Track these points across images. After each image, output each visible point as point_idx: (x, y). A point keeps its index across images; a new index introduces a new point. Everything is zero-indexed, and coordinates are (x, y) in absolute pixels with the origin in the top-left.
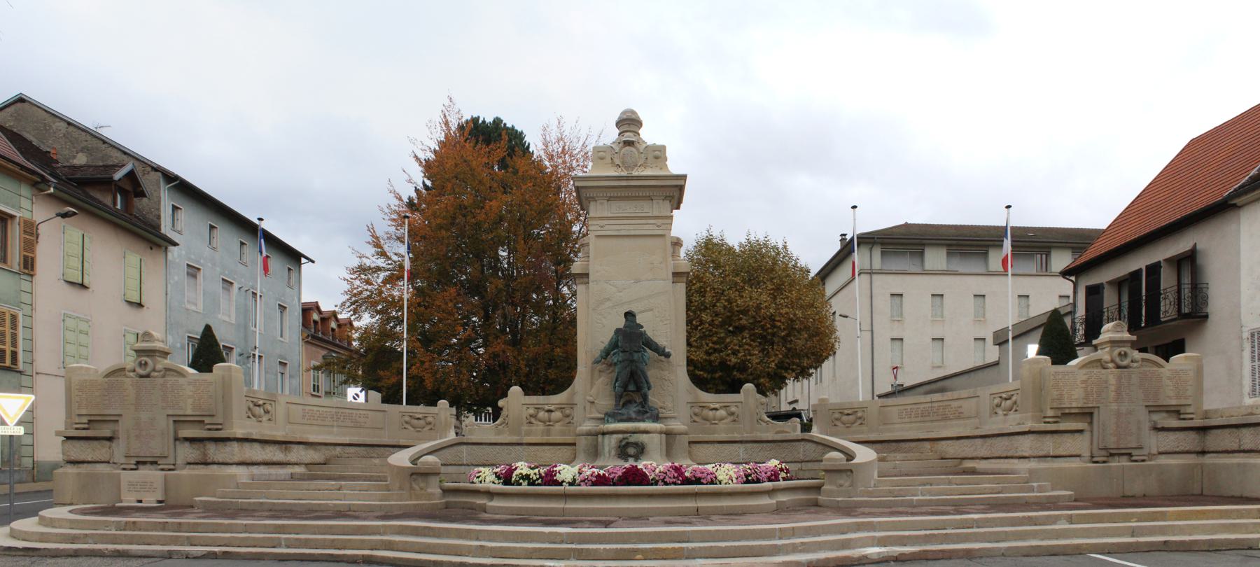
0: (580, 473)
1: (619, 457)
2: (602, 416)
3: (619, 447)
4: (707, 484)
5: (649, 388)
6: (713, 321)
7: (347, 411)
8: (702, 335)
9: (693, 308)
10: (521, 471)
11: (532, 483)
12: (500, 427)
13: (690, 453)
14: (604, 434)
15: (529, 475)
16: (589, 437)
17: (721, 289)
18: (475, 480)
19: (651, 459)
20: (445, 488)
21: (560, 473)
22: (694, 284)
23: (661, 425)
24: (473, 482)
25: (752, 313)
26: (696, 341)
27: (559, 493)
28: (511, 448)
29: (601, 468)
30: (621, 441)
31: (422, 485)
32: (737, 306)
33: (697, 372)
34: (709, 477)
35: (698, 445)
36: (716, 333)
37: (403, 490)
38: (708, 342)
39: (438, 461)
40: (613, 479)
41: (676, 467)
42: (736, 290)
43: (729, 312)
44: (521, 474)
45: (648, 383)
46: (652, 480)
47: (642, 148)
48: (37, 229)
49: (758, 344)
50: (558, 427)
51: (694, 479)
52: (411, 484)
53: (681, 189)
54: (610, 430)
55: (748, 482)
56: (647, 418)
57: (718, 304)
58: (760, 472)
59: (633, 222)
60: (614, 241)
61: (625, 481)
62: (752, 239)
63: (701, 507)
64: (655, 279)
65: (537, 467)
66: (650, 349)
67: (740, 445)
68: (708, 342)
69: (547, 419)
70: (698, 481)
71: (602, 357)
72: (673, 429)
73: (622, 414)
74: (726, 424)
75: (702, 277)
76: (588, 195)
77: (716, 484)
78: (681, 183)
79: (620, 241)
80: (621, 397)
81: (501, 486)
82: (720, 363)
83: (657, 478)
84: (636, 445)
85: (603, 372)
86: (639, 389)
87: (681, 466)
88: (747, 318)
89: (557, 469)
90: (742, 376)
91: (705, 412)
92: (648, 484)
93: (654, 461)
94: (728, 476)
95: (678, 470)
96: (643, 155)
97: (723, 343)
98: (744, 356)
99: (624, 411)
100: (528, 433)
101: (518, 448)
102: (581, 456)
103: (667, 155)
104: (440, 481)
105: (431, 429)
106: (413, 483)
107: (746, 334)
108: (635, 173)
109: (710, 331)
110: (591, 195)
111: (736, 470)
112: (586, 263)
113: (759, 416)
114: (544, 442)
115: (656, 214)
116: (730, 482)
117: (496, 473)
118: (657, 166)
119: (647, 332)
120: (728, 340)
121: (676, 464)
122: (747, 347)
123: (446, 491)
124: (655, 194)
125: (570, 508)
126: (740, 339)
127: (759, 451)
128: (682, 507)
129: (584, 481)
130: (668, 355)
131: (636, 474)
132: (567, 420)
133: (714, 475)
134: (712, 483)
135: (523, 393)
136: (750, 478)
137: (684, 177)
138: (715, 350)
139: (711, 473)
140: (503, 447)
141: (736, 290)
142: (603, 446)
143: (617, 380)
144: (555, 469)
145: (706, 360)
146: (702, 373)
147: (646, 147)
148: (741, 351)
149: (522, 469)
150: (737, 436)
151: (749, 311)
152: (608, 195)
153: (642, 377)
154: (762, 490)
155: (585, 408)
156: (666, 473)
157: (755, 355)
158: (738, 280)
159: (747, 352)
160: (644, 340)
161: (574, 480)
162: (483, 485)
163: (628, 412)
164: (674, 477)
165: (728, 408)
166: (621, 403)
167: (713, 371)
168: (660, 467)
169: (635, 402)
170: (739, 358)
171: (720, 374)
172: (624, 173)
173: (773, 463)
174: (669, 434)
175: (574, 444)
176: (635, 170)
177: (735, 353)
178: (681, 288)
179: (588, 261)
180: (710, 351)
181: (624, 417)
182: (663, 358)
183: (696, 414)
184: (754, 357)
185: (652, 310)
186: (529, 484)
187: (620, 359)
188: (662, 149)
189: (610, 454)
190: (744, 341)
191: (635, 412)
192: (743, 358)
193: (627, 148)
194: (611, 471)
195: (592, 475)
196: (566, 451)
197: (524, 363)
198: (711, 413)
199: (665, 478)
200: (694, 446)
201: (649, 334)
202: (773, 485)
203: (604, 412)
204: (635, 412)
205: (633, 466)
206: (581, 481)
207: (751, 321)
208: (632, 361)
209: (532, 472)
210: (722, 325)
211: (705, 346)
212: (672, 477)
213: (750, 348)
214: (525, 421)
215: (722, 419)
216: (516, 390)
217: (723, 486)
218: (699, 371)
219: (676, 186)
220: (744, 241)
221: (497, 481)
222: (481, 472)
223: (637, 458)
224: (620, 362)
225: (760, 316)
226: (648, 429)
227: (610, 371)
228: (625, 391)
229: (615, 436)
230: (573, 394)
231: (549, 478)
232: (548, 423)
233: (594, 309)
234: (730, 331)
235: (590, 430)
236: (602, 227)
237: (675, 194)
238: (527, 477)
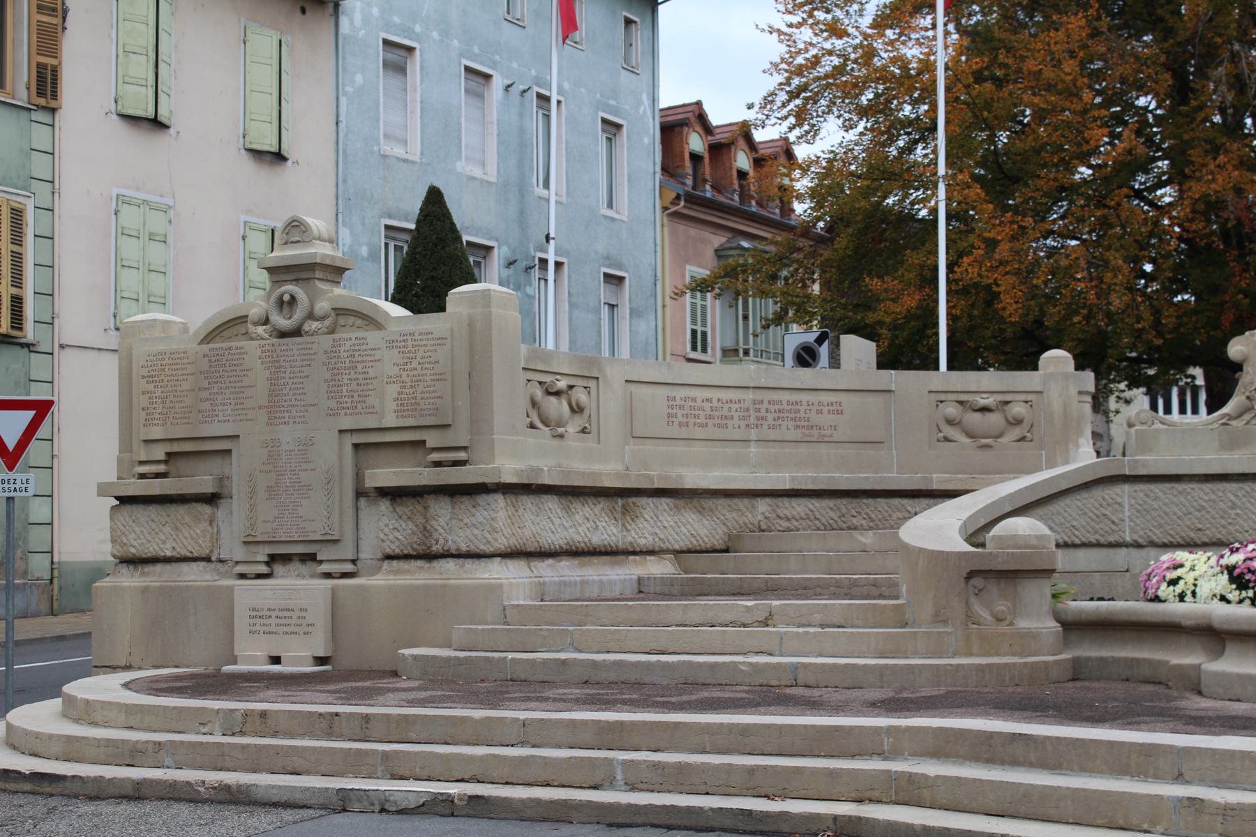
7: (785, 397)
12: (1234, 423)
18: (1164, 591)
20: (1070, 618)
24: (1156, 599)
31: (1001, 607)
37: (945, 622)
39: (1048, 532)
52: (967, 603)
104: (1054, 596)
105: (1023, 439)
106: (973, 600)
117: (1230, 569)
123: (1074, 627)
162: (1188, 607)
221: (1234, 595)
222: (1181, 566)
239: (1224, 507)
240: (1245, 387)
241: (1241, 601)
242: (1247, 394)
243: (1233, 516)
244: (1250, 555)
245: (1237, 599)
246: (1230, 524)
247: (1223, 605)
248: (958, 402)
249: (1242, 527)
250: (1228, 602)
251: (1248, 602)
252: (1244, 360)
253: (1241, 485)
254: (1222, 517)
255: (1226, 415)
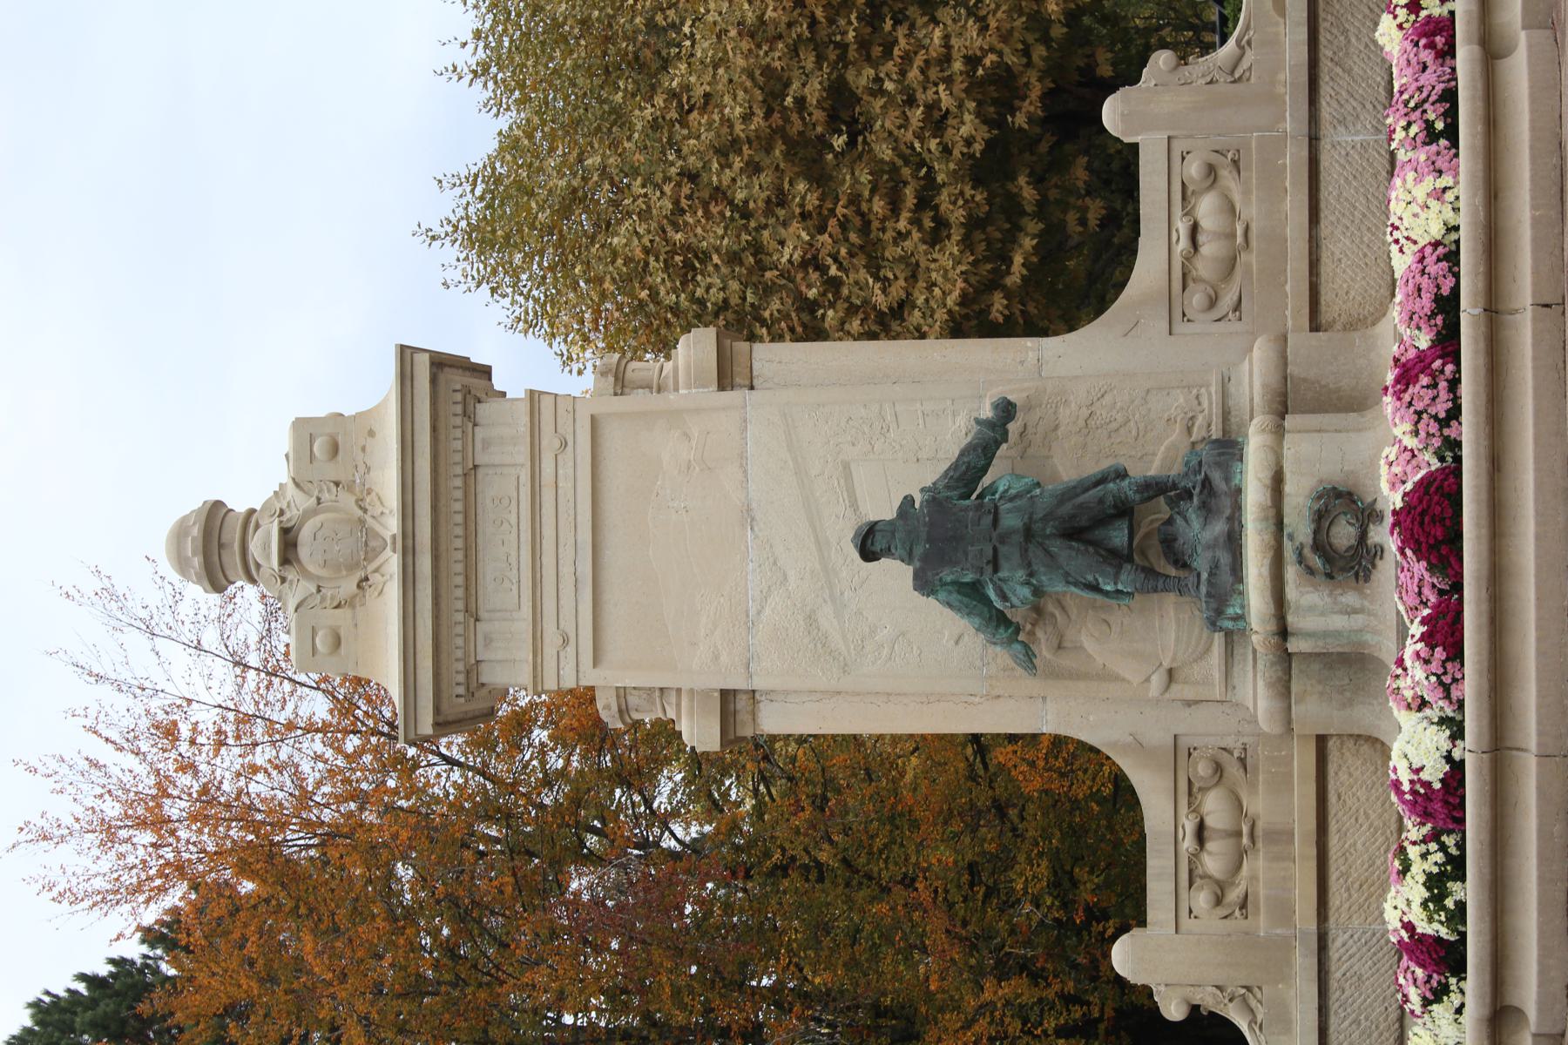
0: (1423, 704)
1: (1367, 579)
2: (1218, 638)
3: (1330, 576)
4: (1457, 276)
5: (1121, 474)
6: (804, 216)
8: (860, 261)
9: (750, 298)
10: (1416, 906)
11: (1456, 868)
13: (1352, 325)
14: (1283, 633)
15: (1429, 876)
16: (1294, 688)
17: (679, 185)
19: (1374, 466)
21: (1422, 768)
22: (654, 295)
23: (1252, 430)
25: (776, 58)
26: (886, 283)
27: (1486, 771)
28: (1336, 975)
29: (1403, 634)
30: (1311, 571)
32: (747, 117)
33: (1014, 278)
34: (1433, 269)
35: (1326, 296)
36: (854, 200)
38: (889, 235)
40: (1441, 592)
41: (1397, 381)
42: (683, 123)
43: (768, 150)
44: (1424, 904)
45: (1102, 480)
46: (1442, 459)
47: (303, 502)
48: (1331, 546)
49: (901, 32)
50: (1258, 804)
51: (1439, 320)
53: (441, 363)
54: (1270, 609)
55: (1452, 133)
56: (1227, 479)
57: (740, 196)
58: (1420, 89)
59: (548, 532)
60: (612, 596)
61: (1444, 550)
62: (469, 58)
63: (1534, 296)
64: (742, 456)
65: (1402, 850)
66: (984, 470)
67: (1325, 145)
68: (889, 235)
69: (1231, 841)
70: (1447, 305)
71: (1013, 639)
72: (1264, 386)
73: (1214, 569)
74: (1246, 193)
75: (628, 261)
76: (461, 690)
77: (1457, 242)
78: (409, 351)
79: (612, 575)
80: (1150, 572)
81: (1470, 984)
82: (977, 183)
83: (1437, 442)
84: (1322, 519)
85: (1061, 637)
86: (1124, 511)
87: (1396, 360)
88: (797, 73)
89: (1405, 777)
90: (1036, 91)
91: (1204, 268)
92: (1457, 472)
93: (1377, 456)
94: (1433, 203)
95: (1407, 374)
96: (326, 496)
97: (894, 170)
98: (949, 81)
99: (1202, 563)
100: (1283, 911)
101: (1334, 953)
102: (1362, 717)
103: (321, 413)
107: (860, 79)
108: (392, 525)
109: (844, 225)
110: (461, 678)
111: (1411, 176)
112: (684, 703)
113: (1222, 78)
114: (1313, 852)
115: (522, 454)
116: (1449, 196)
117: (1426, 1003)
118: (363, 449)
119: (929, 483)
120: (885, 152)
121: (1390, 378)
122: (914, 74)
124: (458, 457)
125: (1540, 733)
126: (880, 102)
127: (1349, 72)
128: (1535, 358)
129: (1446, 689)
130: (1007, 410)
131: (1422, 514)
132: (1233, 770)
133: (1429, 250)
134: (1452, 257)
135: (1136, 932)
136: (1440, 125)
137: (406, 353)
138: (925, 202)
139: (1421, 260)
140: (1334, 1006)
141: (683, 123)
142: (1326, 634)
143: (1095, 588)
144: (1406, 787)
145: (967, 243)
146: (1018, 260)
147: (297, 485)
148: (930, 95)
149: (1409, 902)
150: (1293, 157)
151: (767, 71)
152: (460, 617)
153: (1082, 499)
154: (1480, 85)
155: (1189, 703)
156: (1419, 414)
157: (947, 37)
158: (643, 115)
159: (934, 73)
160: (955, 493)
161: (1443, 721)
163: (1208, 547)
164: (1434, 386)
165: (1190, 188)
166: (1173, 572)
167: (1012, 209)
168: (1398, 432)
169: (1170, 522)
170: (960, 106)
171: (1022, 180)
172: (392, 562)
173: (1390, 35)
174: (1283, 404)
175: (1322, 741)
176: (378, 528)
177: (937, 121)
178: (772, 358)
179: (679, 690)
180: (928, 224)
181: (1225, 558)
182: (1013, 427)
183: (1213, 303)
184: (955, 42)
185: (846, 466)
186: (1462, 878)
187: (1021, 574)
188: (305, 430)
189: (1355, 611)
190: (889, 86)
191: (1206, 522)
192: (959, 87)
193: (303, 552)
194: (1413, 601)
195: (1427, 662)
196: (1346, 772)
197: (989, 984)
198: (1208, 248)
199: (1435, 417)
200: (1328, 312)
201: (931, 474)
202: (1469, 41)
203: (1206, 633)
204: (1206, 522)
205: (1394, 526)
206: (1447, 696)
207: (809, 61)
208: (1028, 533)
209: (1418, 869)
210: (821, 179)
211: (907, 244)
212: (1431, 393)
213: (919, 61)
214: (1238, 923)
215: (1231, 210)
216: (1124, 957)
217: (1463, 220)
218: (1008, 273)
219: (434, 381)
220: (480, 92)
221: (1456, 999)
223: (1367, 515)
224: (1031, 575)
225: (790, 25)
226: (1266, 476)
227: (1057, 613)
228: (1130, 559)
229: (1291, 593)
230: (1138, 747)
231: (1438, 806)
232: (1245, 840)
233: (845, 669)
234: (852, 143)
235: (1270, 685)
236: (566, 641)
237: (458, 387)
238: (1437, 885)
239: (1357, 1033)
240: (1218, 1003)
241: (1462, 992)
242: (1226, 1001)
243: (1368, 1023)
244: (1411, 981)
245: (1459, 995)
246: (1377, 1027)
247: (1466, 1011)
248: (1184, 289)
249: (1381, 1014)
250: (1463, 1005)
251: (1462, 984)
252: (1188, 1003)
253: (1332, 1013)
254: (1370, 1036)
255: (1250, 1026)
